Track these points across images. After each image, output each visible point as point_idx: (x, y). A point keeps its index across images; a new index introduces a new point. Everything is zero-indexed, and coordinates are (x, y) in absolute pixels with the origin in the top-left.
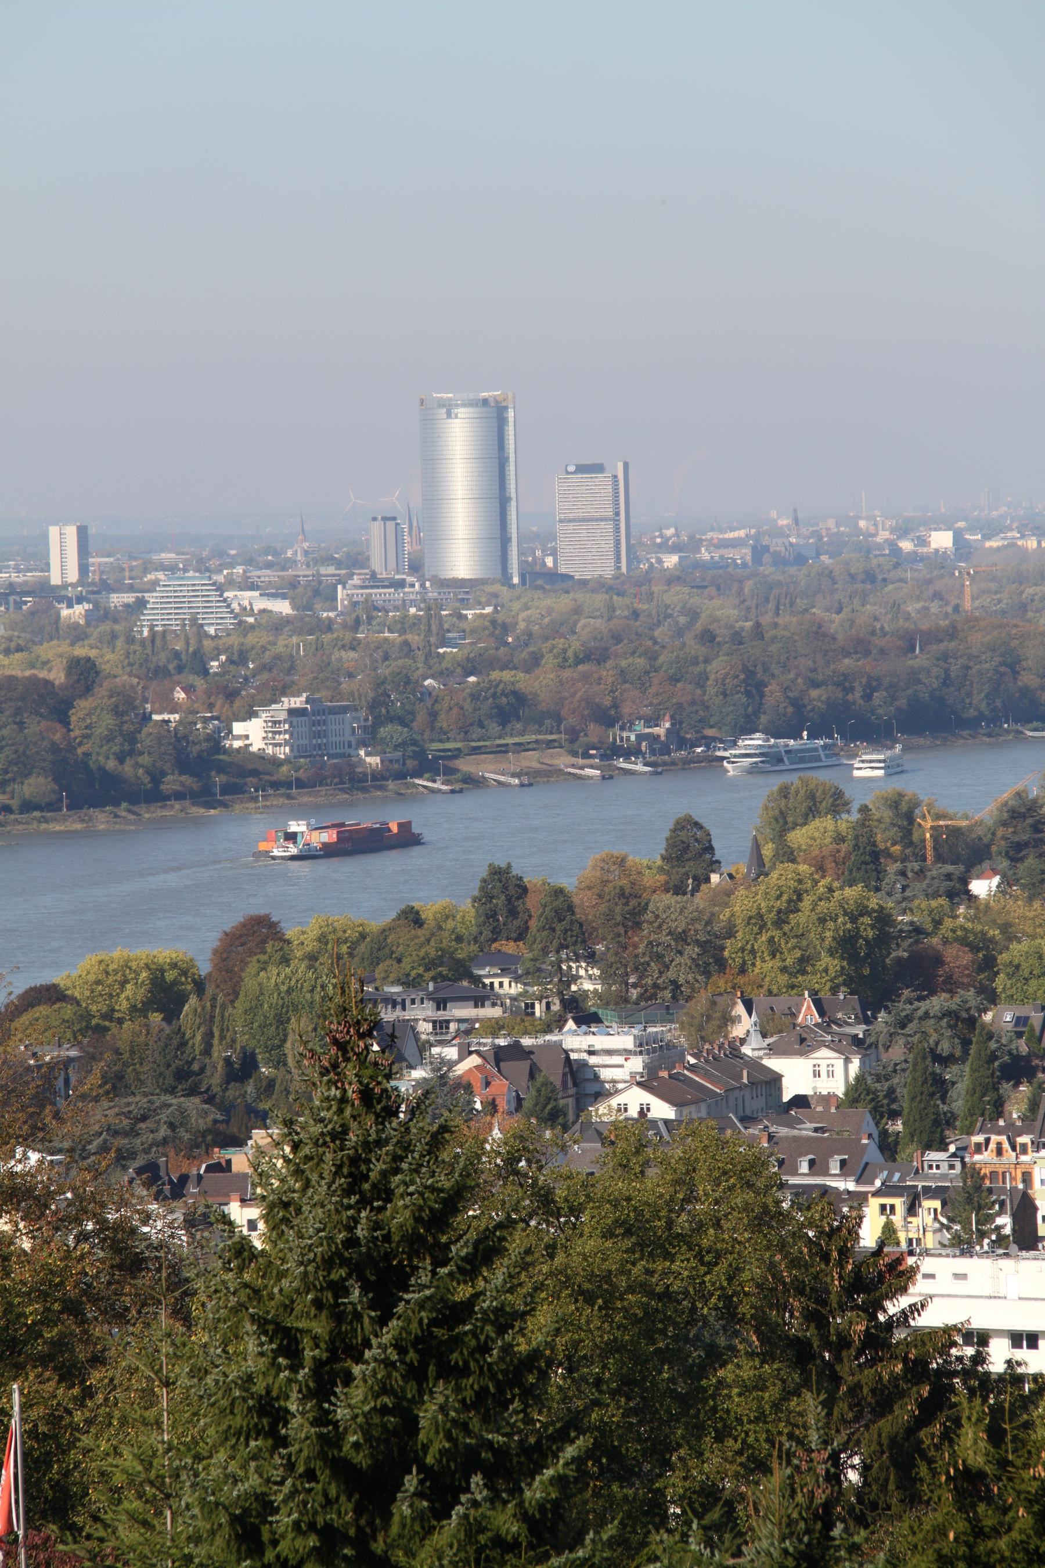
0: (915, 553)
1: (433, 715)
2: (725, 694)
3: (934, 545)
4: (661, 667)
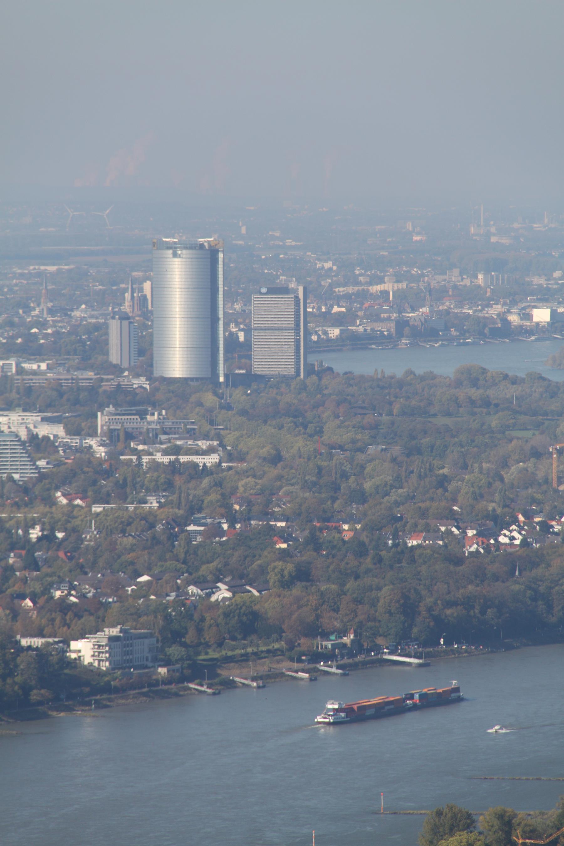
0: (521, 327)
1: (200, 631)
2: (390, 613)
3: (536, 319)
4: (348, 591)
